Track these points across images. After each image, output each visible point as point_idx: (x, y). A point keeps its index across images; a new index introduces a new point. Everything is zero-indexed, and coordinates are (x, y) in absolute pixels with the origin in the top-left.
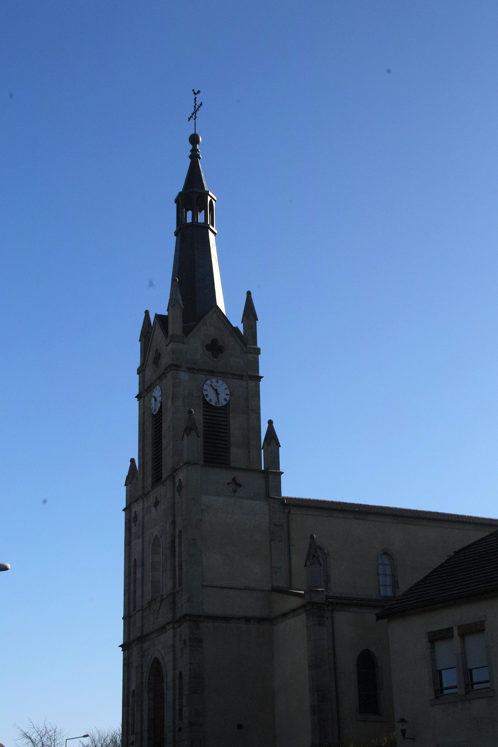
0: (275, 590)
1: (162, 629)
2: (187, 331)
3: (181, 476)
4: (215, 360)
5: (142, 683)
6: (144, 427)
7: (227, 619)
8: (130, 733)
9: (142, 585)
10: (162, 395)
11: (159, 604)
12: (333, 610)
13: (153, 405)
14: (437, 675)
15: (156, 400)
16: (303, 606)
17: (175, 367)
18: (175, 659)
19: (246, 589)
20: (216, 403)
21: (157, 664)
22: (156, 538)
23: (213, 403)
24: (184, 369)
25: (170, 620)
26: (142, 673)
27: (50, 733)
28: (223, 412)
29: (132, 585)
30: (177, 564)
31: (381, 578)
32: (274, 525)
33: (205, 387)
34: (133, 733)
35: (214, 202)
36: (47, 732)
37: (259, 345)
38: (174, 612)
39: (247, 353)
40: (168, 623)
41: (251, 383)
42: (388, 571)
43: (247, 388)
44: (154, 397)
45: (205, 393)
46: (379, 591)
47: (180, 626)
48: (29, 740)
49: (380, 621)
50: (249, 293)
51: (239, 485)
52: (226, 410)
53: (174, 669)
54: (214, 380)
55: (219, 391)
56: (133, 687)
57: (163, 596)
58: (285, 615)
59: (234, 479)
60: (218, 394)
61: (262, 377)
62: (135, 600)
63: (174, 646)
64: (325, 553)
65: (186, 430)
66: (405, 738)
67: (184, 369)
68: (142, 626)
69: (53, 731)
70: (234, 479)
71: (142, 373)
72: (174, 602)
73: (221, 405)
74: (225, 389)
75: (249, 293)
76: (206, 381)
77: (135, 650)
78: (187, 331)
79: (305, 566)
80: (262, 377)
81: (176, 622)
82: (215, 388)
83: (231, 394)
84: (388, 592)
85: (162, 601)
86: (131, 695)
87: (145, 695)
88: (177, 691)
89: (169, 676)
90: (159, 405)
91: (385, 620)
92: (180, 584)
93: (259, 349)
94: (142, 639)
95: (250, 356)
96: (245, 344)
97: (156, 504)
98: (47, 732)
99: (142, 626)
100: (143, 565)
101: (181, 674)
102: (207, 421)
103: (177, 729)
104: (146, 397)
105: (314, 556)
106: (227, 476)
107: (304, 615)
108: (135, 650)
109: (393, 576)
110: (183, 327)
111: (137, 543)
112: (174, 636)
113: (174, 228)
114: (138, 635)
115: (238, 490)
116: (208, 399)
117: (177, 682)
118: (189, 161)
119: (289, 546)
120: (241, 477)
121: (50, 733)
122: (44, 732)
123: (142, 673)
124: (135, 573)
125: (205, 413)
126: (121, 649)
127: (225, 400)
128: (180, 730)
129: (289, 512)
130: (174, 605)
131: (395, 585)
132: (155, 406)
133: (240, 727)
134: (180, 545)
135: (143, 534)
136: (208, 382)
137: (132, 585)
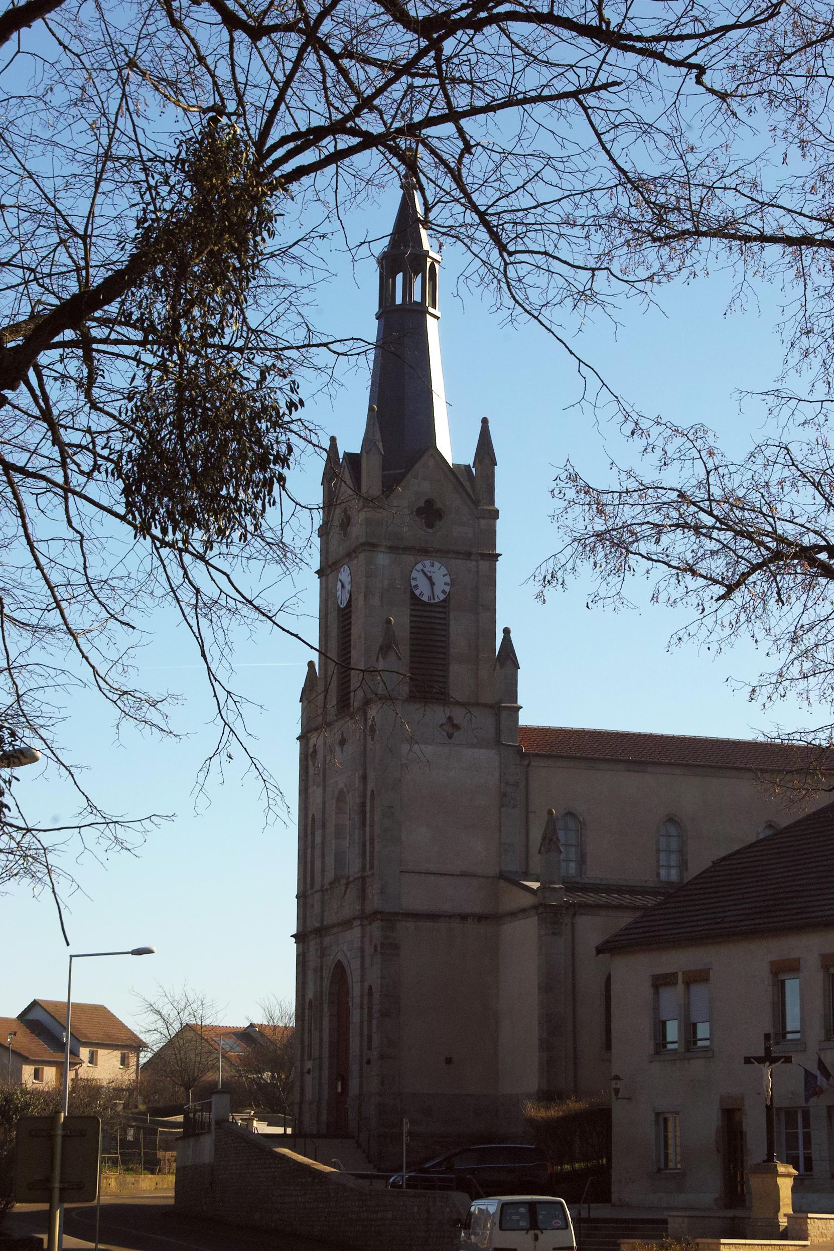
0: (503, 876)
1: (346, 924)
2: (389, 485)
3: (372, 712)
4: (430, 531)
5: (321, 992)
6: (326, 623)
7: (434, 917)
8: (306, 1057)
9: (323, 856)
10: (351, 582)
11: (343, 888)
12: (574, 915)
13: (339, 593)
14: (660, 1028)
15: (343, 586)
16: (535, 907)
17: (371, 546)
18: (363, 967)
19: (464, 874)
20: (429, 598)
21: (340, 970)
22: (341, 791)
23: (425, 598)
24: (383, 550)
25: (357, 913)
26: (322, 978)
27: (194, 1006)
28: (440, 610)
29: (309, 850)
30: (368, 837)
31: (663, 856)
32: (506, 783)
33: (414, 574)
34: (310, 1058)
35: (437, 265)
36: (188, 1004)
37: (497, 505)
38: (363, 904)
39: (478, 518)
40: (354, 919)
41: (484, 565)
42: (674, 844)
43: (478, 572)
44: (341, 581)
45: (413, 583)
46: (658, 875)
47: (370, 923)
48: (159, 1017)
49: (601, 955)
50: (485, 421)
51: (456, 727)
52: (444, 607)
53: (362, 981)
54: (428, 563)
55: (434, 580)
56: (310, 995)
57: (349, 877)
58: (513, 915)
59: (450, 719)
60: (432, 584)
61: (500, 555)
62: (312, 878)
63: (362, 949)
64: (579, 821)
65: (381, 648)
66: (617, 1098)
67: (383, 550)
68: (323, 912)
69: (200, 1003)
70: (450, 719)
71: (324, 537)
72: (363, 891)
73: (437, 600)
74: (444, 576)
75: (485, 421)
76: (416, 564)
77: (313, 944)
78: (389, 485)
79: (539, 853)
80: (500, 555)
81: (366, 917)
82: (429, 574)
83: (453, 583)
84: (674, 875)
85: (348, 884)
86: (307, 1006)
87: (326, 1009)
88: (366, 1011)
89: (356, 989)
90: (348, 596)
91: (608, 955)
92: (372, 867)
93: (497, 511)
94: (321, 931)
95: (483, 522)
96: (476, 503)
97: (343, 742)
98: (188, 1004)
99: (323, 912)
100: (324, 826)
101: (370, 988)
102: (415, 619)
103: (365, 1061)
104: (330, 576)
105: (551, 840)
106: (438, 714)
107: (536, 918)
108: (313, 944)
109: (682, 852)
110: (384, 476)
111: (316, 793)
112: (363, 936)
113: (376, 308)
114: (317, 925)
115: (455, 734)
116: (417, 593)
117: (366, 1000)
118: (401, 192)
119: (527, 812)
120: (458, 714)
121: (194, 1006)
122: (183, 1004)
123: (322, 978)
124: (313, 834)
125: (414, 613)
126: (293, 940)
127: (444, 592)
128: (368, 1062)
129: (529, 765)
130: (363, 895)
131: (683, 865)
132: (342, 597)
133: (449, 1061)
134: (372, 811)
135: (324, 780)
136: (419, 566)
137: (309, 850)
